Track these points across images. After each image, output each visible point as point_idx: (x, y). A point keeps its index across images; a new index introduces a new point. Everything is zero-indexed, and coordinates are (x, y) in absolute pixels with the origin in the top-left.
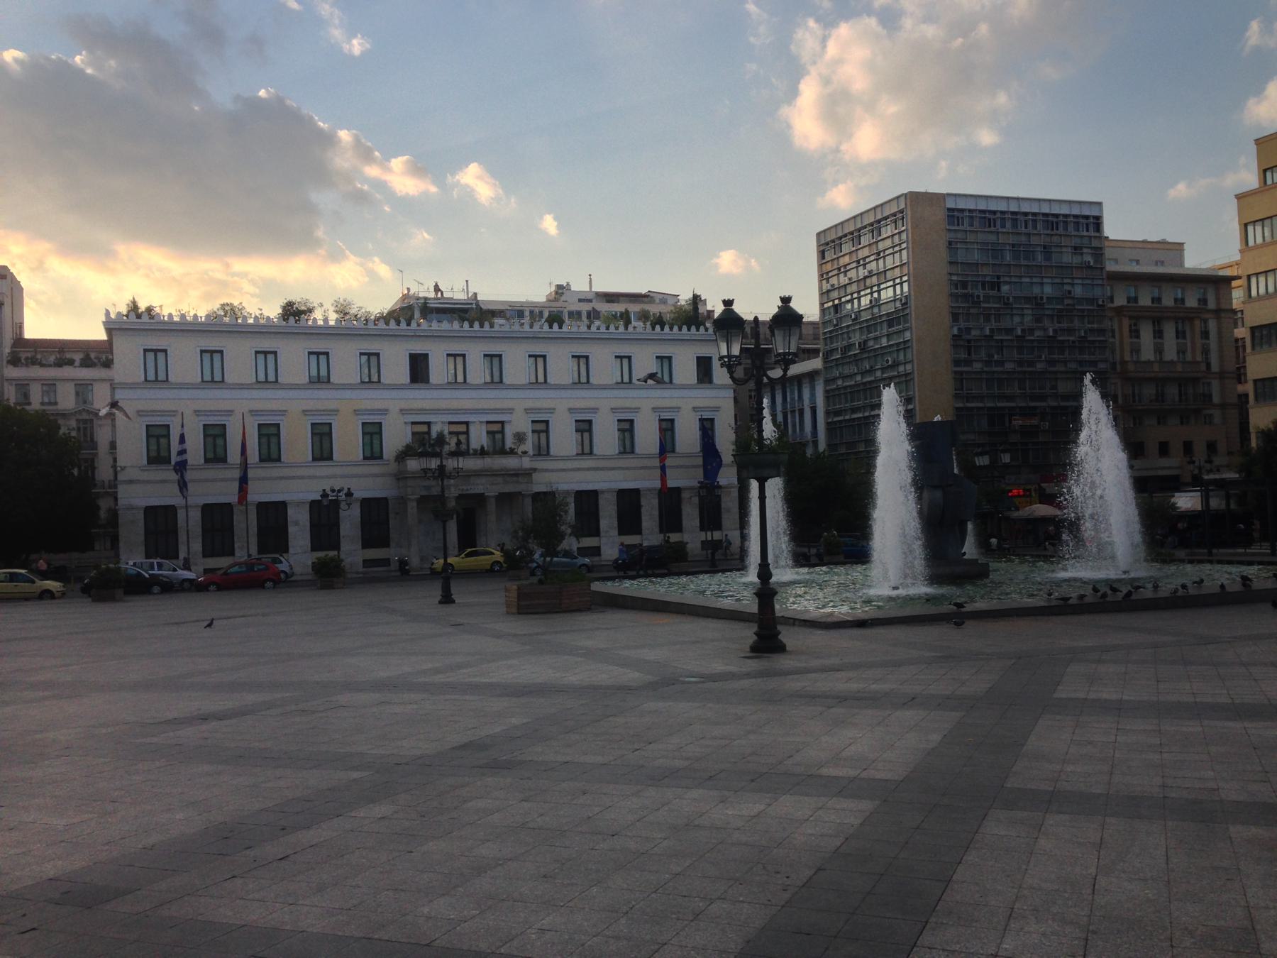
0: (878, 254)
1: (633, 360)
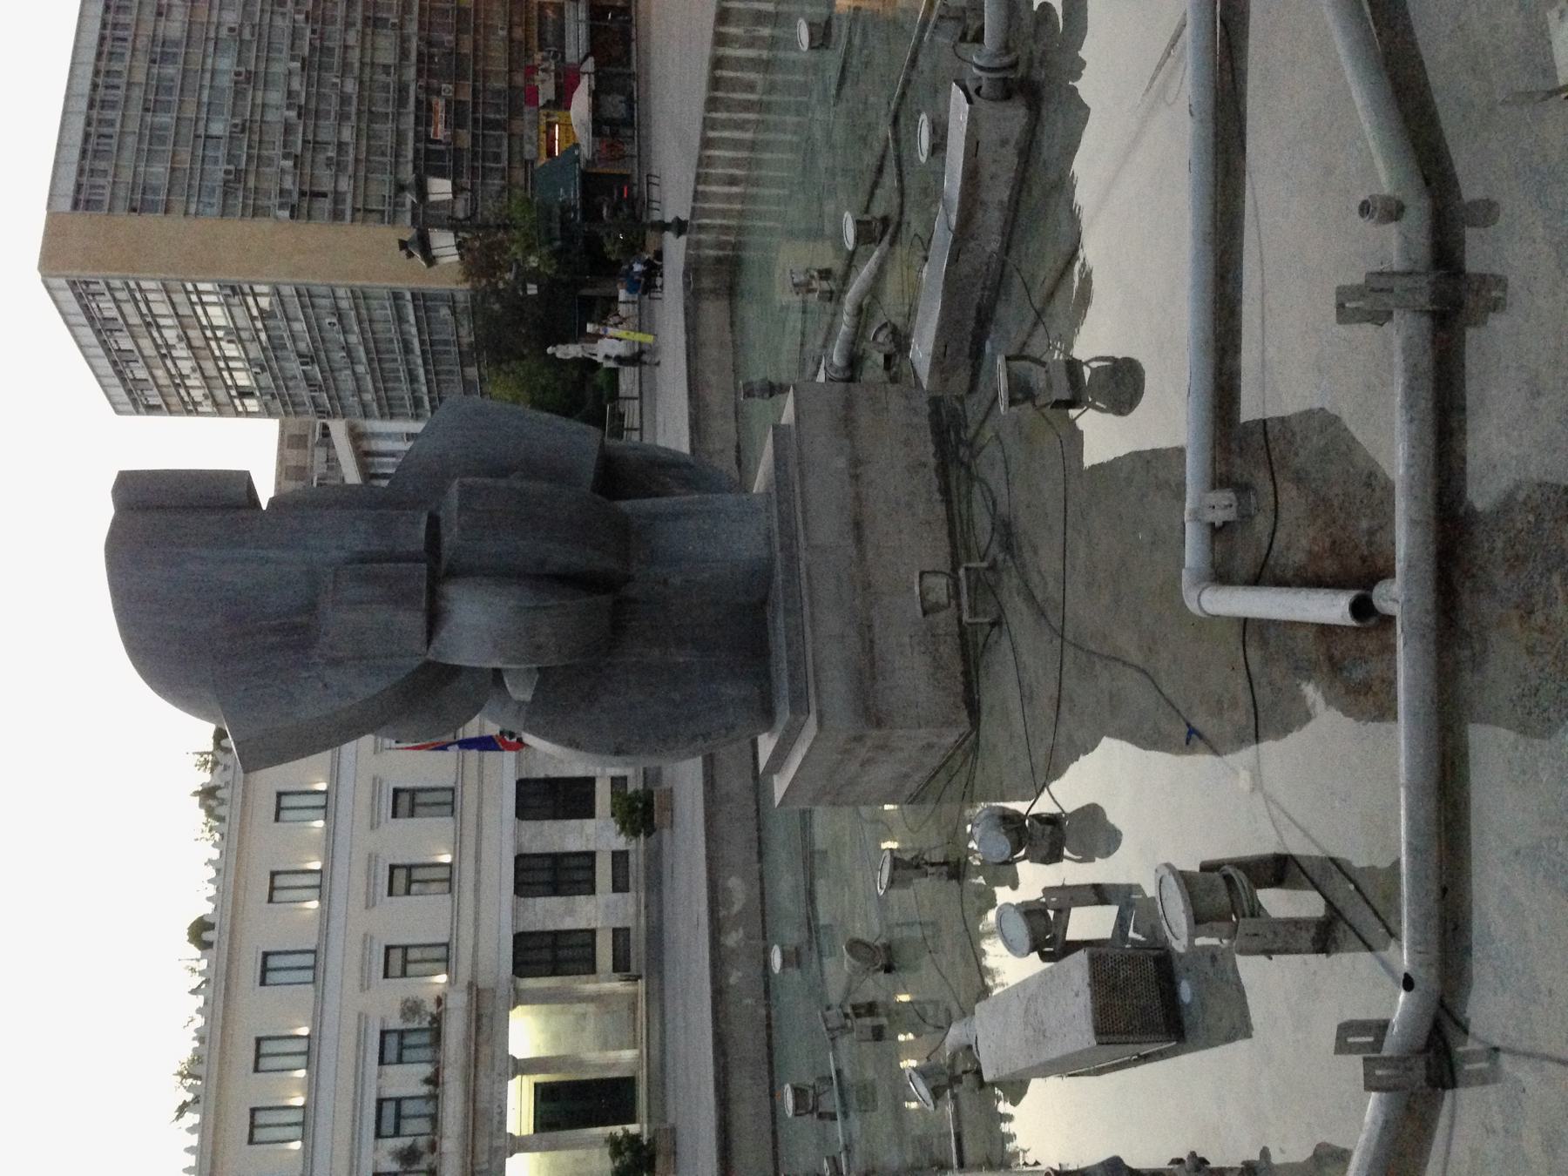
0: (148, 325)
1: (282, 788)
